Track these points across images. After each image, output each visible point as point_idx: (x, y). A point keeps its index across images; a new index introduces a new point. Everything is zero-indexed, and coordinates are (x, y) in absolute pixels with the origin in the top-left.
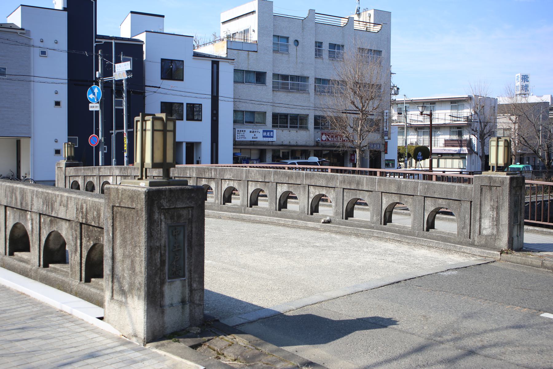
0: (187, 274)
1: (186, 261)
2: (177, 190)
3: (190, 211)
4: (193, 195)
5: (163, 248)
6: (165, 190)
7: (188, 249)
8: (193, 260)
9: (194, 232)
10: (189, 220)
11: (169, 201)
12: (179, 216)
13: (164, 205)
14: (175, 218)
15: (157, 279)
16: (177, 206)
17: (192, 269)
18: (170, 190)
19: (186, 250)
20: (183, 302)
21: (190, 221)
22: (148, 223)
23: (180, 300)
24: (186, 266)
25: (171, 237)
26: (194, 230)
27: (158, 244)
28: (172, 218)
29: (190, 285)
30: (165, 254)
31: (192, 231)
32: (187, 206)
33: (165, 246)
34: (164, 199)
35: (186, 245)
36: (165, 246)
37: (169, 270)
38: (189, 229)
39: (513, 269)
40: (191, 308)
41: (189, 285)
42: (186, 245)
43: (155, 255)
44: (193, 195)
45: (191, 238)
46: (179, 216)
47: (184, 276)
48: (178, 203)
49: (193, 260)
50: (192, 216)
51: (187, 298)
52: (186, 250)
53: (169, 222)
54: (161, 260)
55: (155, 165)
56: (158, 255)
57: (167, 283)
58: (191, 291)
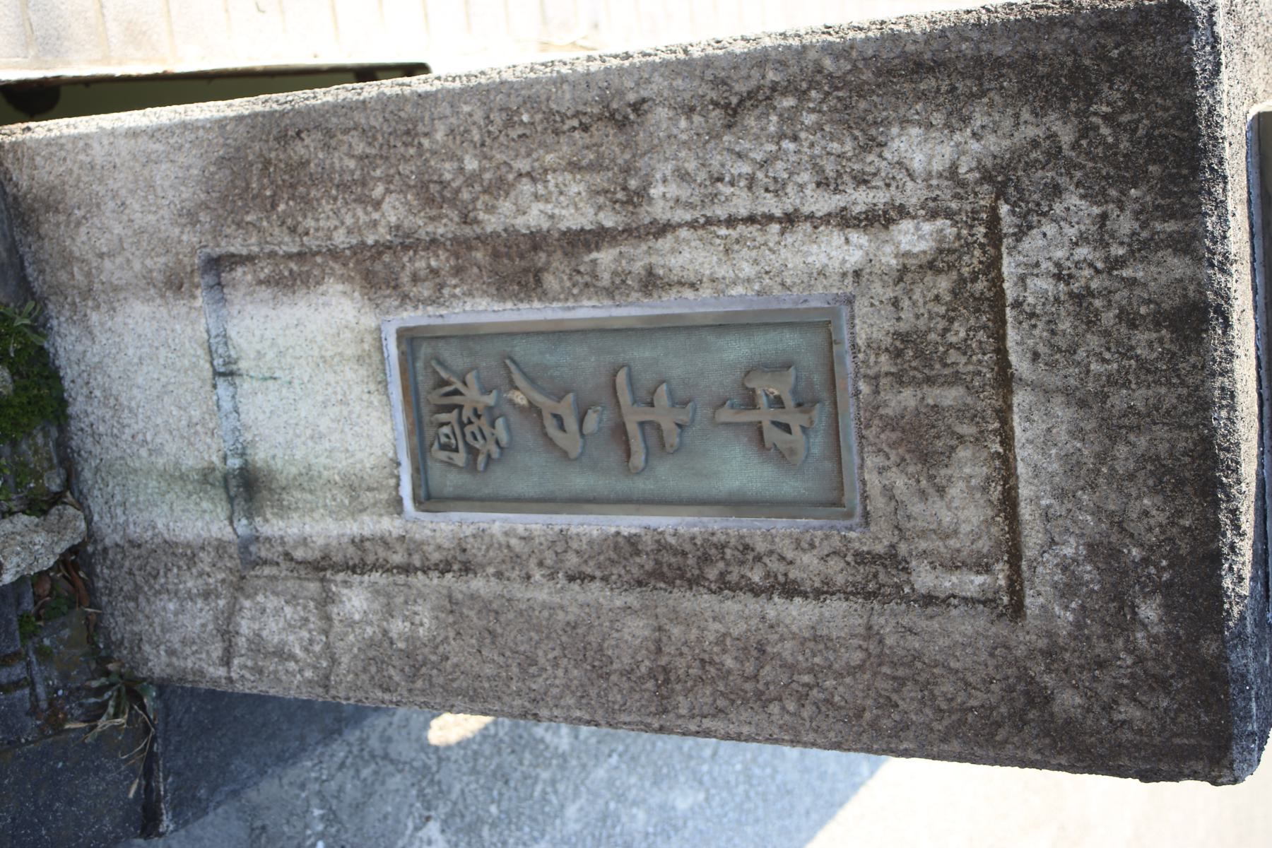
0: (444, 527)
1: (536, 523)
2: (1201, 404)
3: (974, 583)
4: (1149, 611)
5: (639, 257)
6: (1194, 244)
7: (633, 543)
8: (542, 593)
9: (777, 607)
10: (893, 560)
11: (1080, 298)
12: (922, 444)
13: (1033, 243)
14: (907, 398)
15: (394, 212)
16: (1021, 398)
17: (477, 584)
18: (1196, 318)
19: (628, 523)
20: (247, 486)
21: (878, 576)
22: (842, 51)
23: (260, 456)
24: (497, 523)
25: (737, 350)
26: (798, 613)
27: (664, 197)
28: (912, 354)
29: (359, 560)
30: (590, 285)
31: (791, 590)
32: (1033, 539)
33: (651, 282)
34: (1101, 234)
35: (665, 522)
36: (651, 282)
37: (468, 336)
38: (808, 566)
39: (1247, 581)
40: (206, 557)
41: (359, 543)
42: (665, 522)
43: (574, 167)
44: (1149, 611)
45: (724, 586)
46: (922, 444)
47: (428, 499)
48: (1062, 412)
49: (542, 593)
50: (929, 600)
51: (273, 526)
52: (628, 523)
53: (870, 325)
54: (537, 240)
55: (1253, 750)
56: (565, 204)
57: (369, 320)
58: (323, 566)
